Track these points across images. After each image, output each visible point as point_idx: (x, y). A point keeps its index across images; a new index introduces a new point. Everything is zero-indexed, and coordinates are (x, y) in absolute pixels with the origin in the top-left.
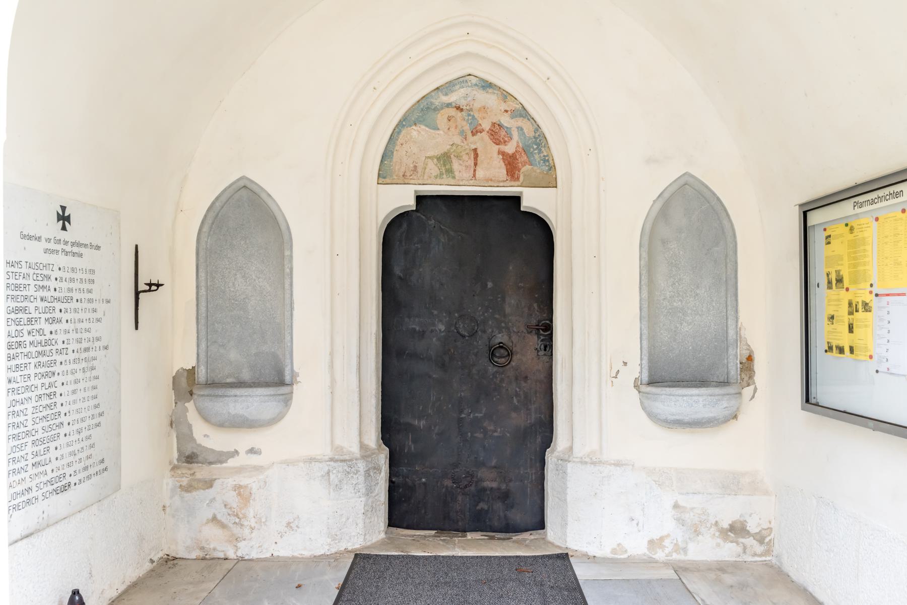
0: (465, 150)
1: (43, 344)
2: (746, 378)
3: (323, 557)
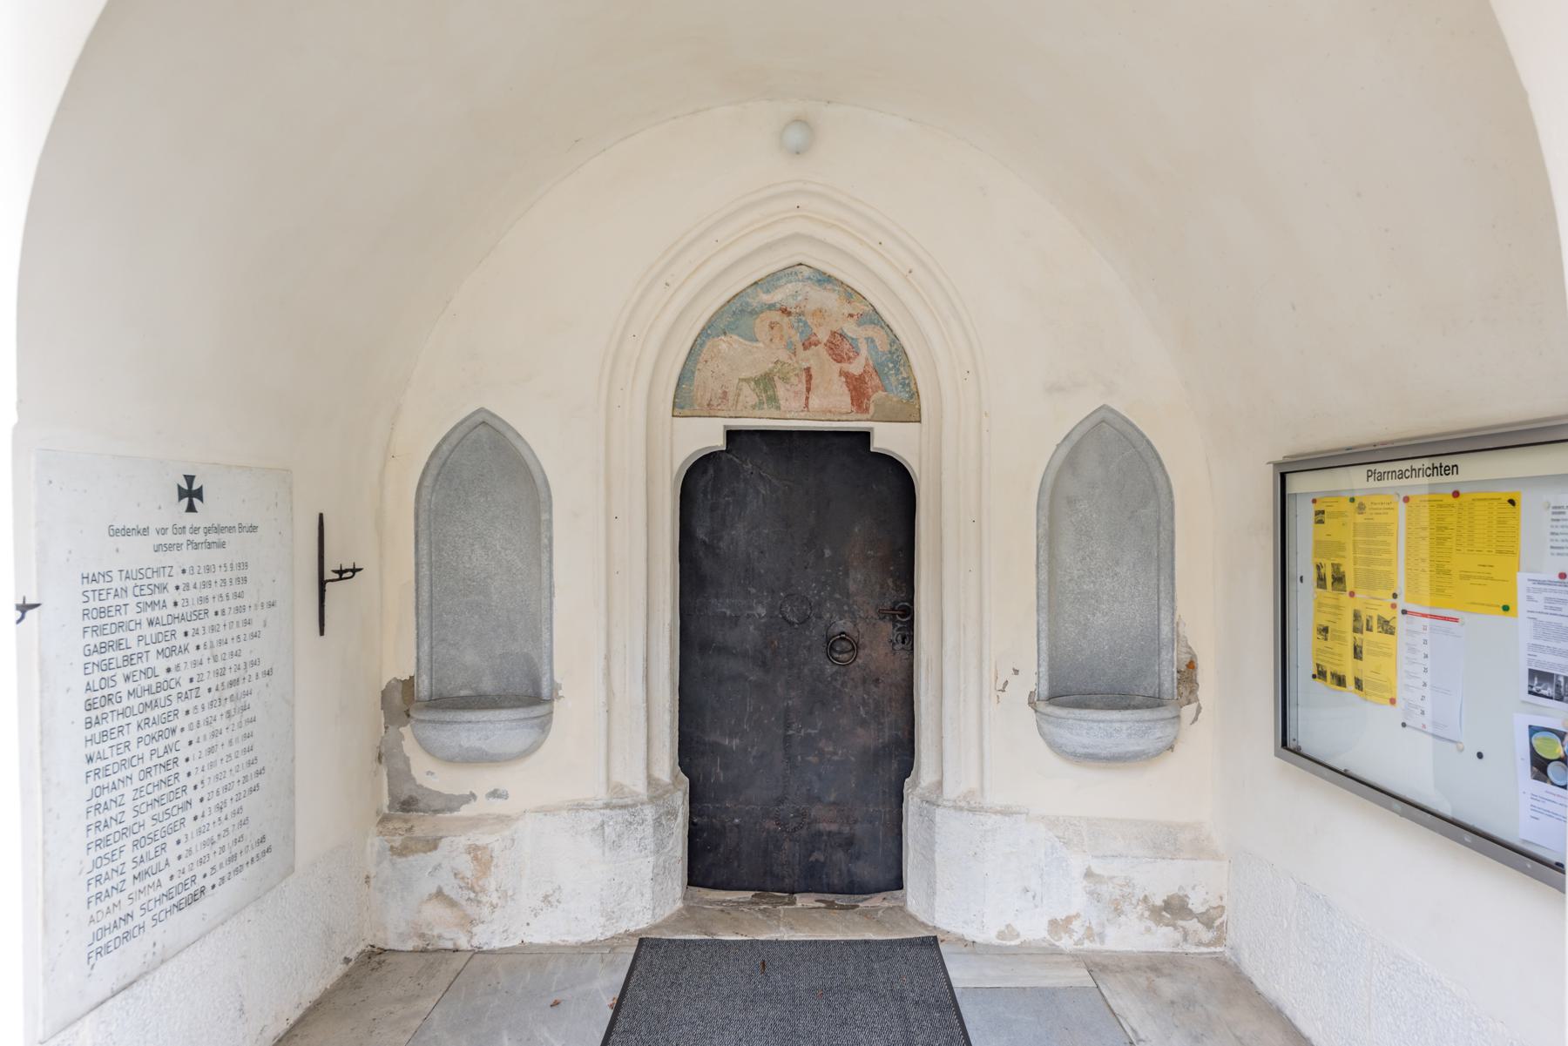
0: (794, 369)
1: (154, 690)
2: (1186, 693)
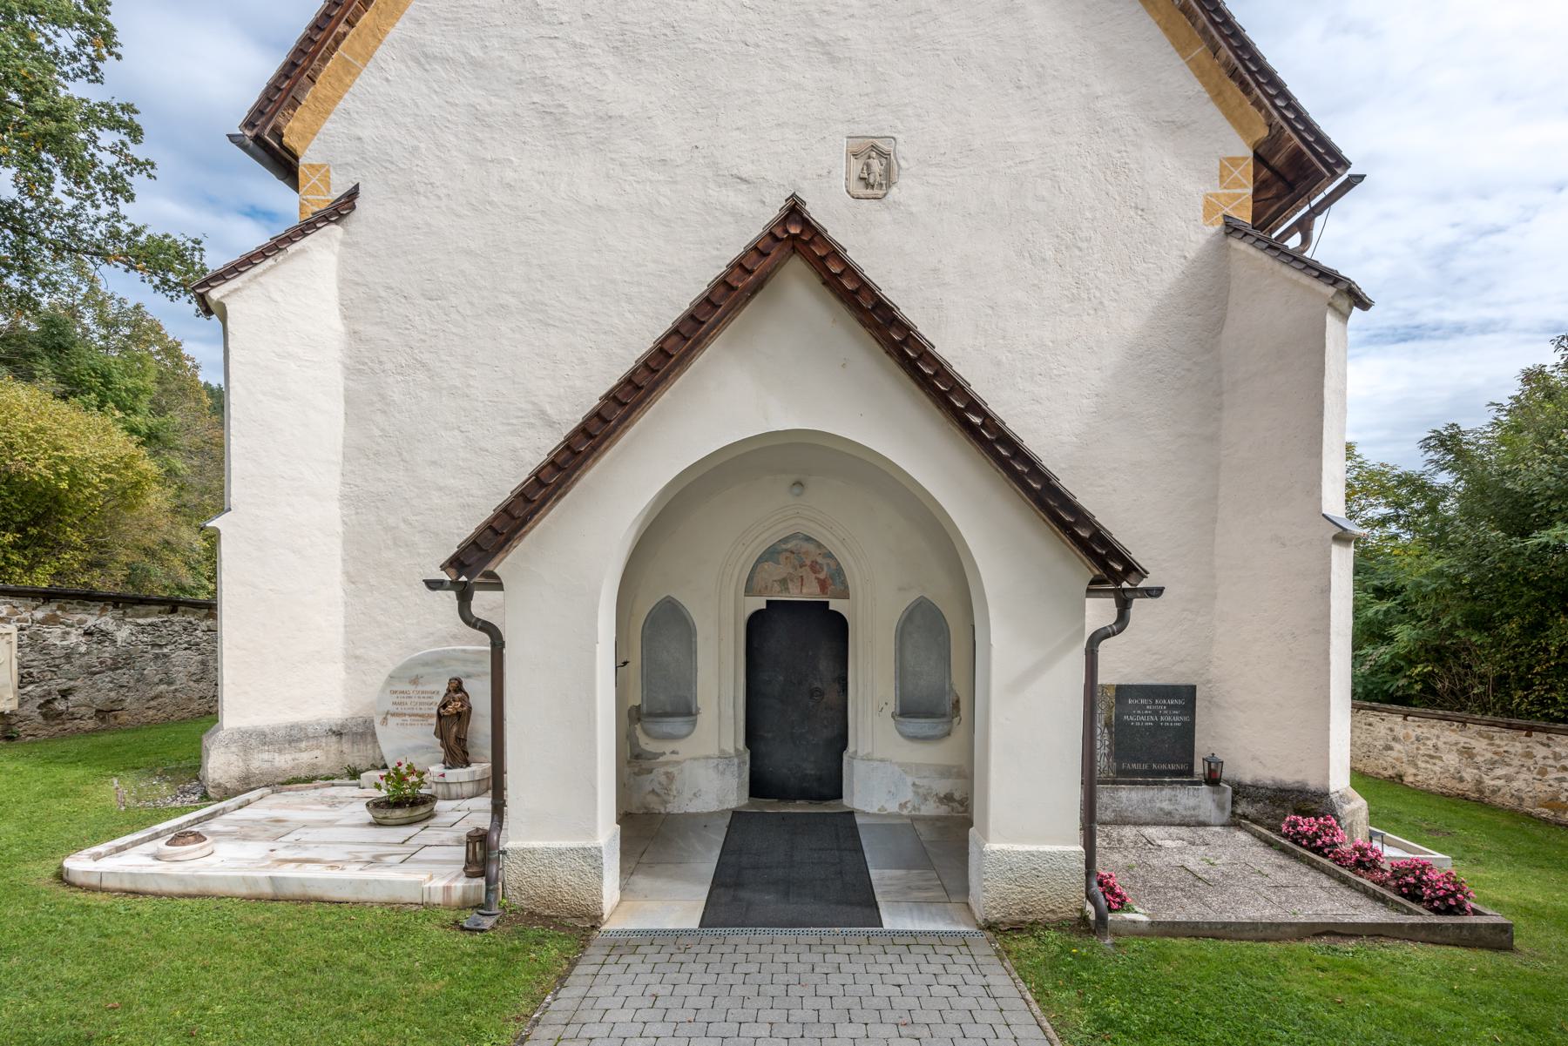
3: (715, 812)
